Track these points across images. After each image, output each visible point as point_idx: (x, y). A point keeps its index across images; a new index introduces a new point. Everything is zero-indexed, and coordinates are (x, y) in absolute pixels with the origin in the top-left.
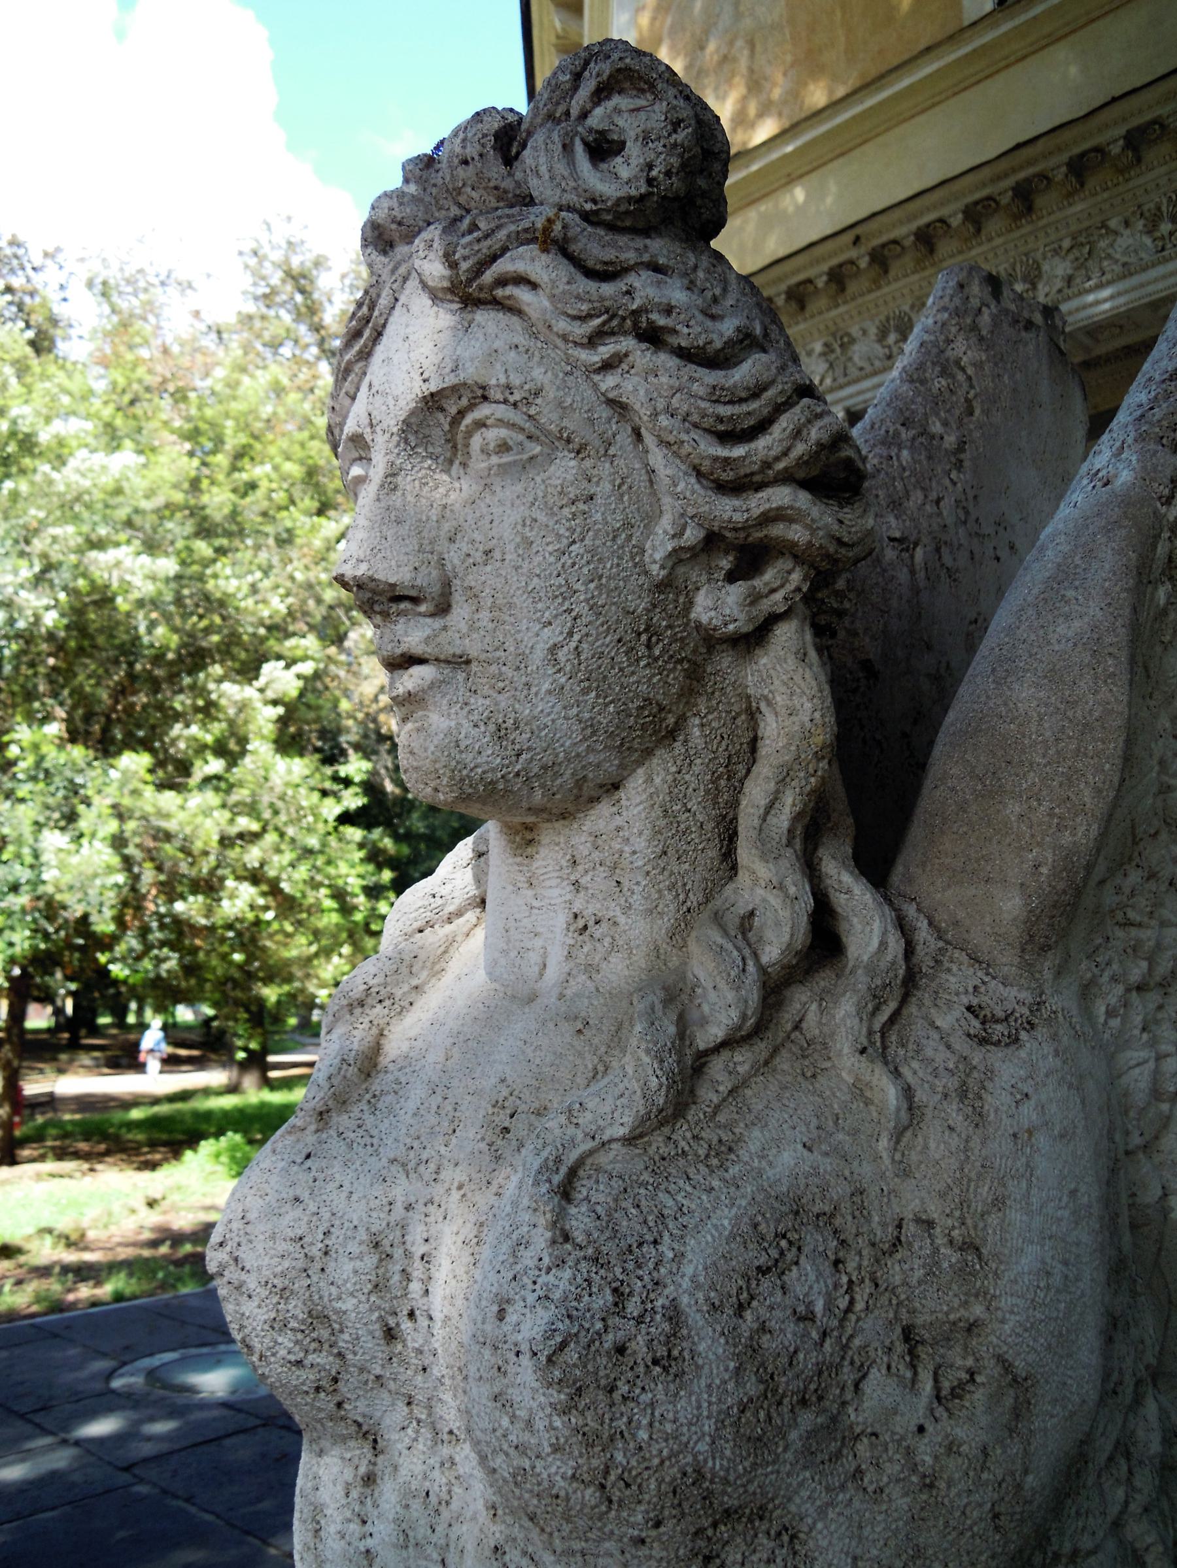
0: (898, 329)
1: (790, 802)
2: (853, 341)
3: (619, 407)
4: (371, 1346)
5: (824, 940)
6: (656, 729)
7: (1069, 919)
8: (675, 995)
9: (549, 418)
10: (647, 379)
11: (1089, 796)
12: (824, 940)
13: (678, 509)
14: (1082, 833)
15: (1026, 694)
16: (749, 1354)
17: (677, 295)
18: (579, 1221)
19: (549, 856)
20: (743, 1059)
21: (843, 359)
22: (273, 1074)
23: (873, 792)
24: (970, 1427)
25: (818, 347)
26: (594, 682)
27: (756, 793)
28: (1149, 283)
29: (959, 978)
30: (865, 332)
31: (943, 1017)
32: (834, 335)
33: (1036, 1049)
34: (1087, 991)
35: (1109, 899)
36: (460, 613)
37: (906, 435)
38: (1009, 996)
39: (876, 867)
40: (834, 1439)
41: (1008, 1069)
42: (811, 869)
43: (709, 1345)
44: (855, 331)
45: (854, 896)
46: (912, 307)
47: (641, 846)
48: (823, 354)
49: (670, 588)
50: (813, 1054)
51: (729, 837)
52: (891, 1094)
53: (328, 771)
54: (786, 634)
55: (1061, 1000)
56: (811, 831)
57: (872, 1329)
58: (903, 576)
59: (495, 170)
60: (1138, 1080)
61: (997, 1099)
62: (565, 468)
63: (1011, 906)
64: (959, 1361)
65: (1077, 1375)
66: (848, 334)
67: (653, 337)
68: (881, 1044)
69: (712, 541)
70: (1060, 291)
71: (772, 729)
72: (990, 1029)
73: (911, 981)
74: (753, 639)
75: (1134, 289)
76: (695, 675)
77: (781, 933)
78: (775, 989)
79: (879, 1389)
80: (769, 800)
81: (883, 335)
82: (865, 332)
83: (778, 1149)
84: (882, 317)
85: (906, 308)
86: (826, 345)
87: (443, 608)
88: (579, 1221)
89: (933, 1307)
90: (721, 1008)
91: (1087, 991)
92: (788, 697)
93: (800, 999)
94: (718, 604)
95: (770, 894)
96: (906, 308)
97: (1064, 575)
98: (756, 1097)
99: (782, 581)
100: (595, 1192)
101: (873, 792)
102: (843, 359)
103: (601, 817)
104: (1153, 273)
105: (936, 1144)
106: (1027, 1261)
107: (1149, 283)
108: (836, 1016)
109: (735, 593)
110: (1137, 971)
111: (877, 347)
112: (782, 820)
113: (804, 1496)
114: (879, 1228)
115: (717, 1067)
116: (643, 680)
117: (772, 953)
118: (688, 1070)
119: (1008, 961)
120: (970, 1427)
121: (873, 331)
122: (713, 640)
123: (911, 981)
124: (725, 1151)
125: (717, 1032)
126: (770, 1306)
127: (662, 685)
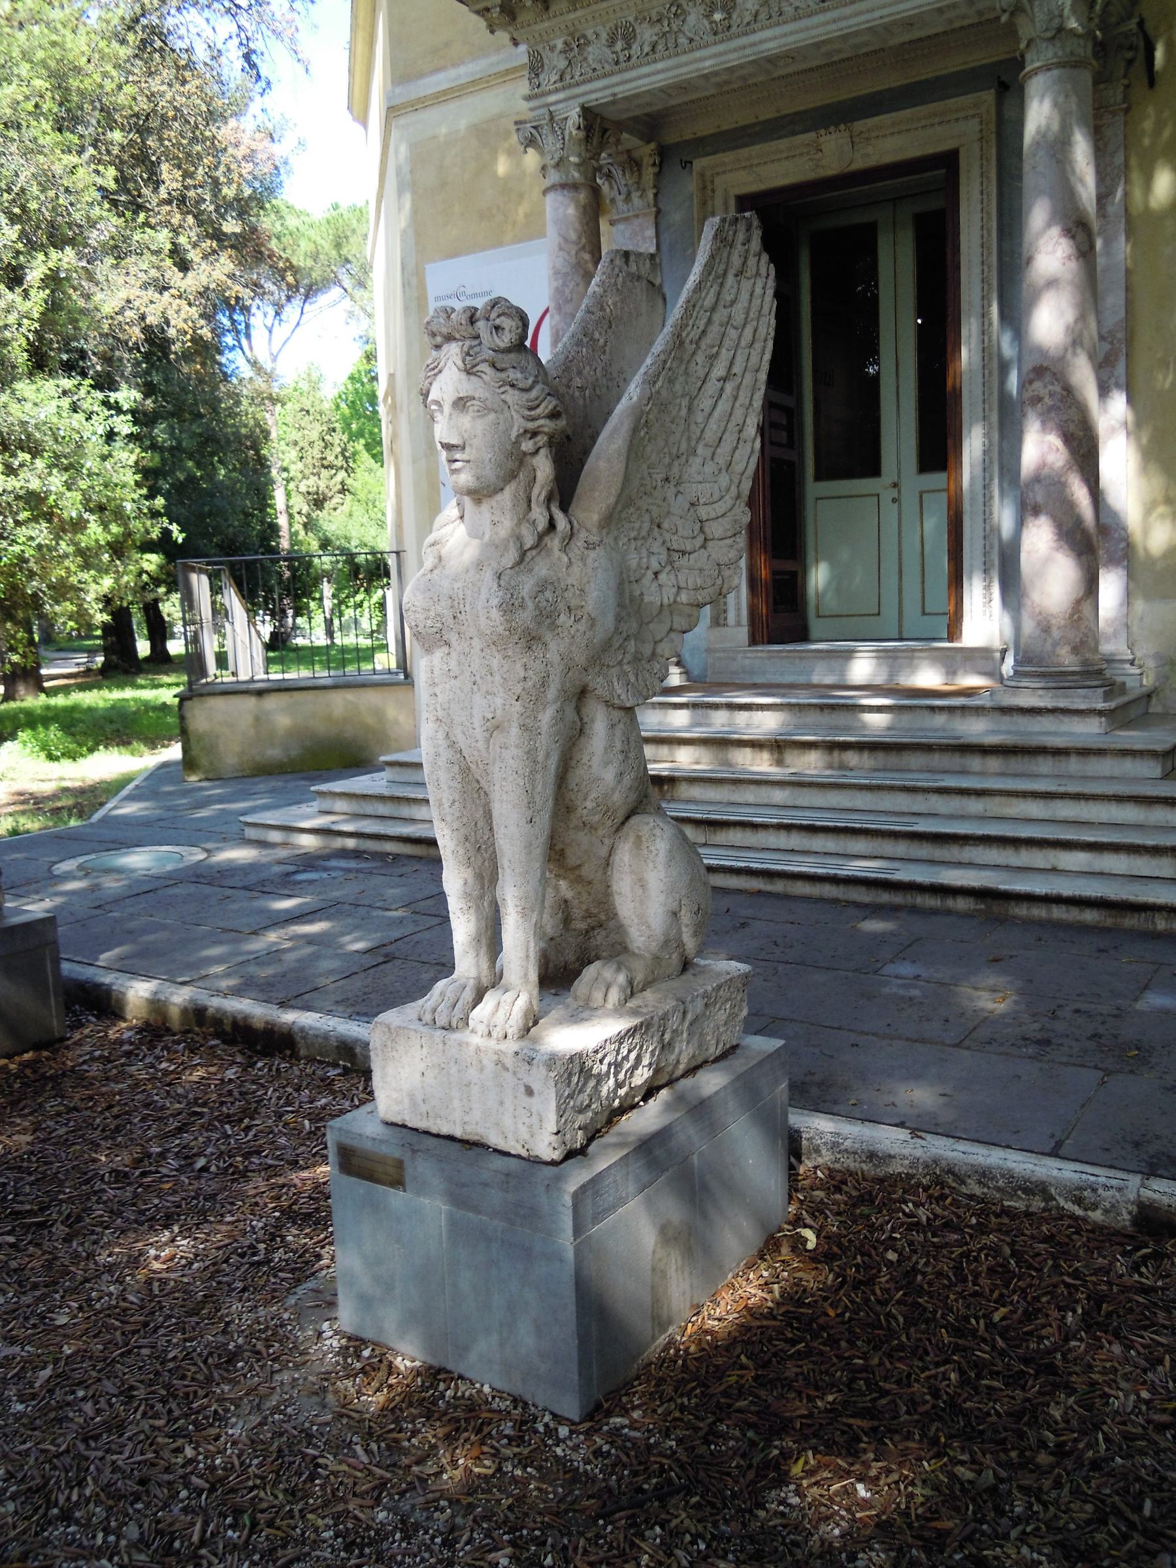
0: (624, 37)
1: (544, 494)
2: (588, 43)
3: (505, 402)
4: (451, 621)
5: (552, 526)
6: (512, 476)
7: (609, 521)
8: (519, 538)
9: (488, 403)
10: (512, 396)
11: (614, 491)
12: (552, 526)
13: (519, 425)
14: (612, 500)
15: (602, 464)
16: (537, 607)
17: (519, 375)
18: (502, 583)
19: (485, 506)
20: (534, 552)
21: (580, 58)
22: (46, 684)
23: (564, 491)
24: (582, 626)
25: (560, 44)
26: (500, 466)
27: (535, 491)
28: (813, 28)
29: (583, 535)
30: (597, 35)
31: (579, 543)
32: (572, 34)
33: (600, 551)
34: (616, 539)
35: (624, 515)
36: (468, 449)
37: (585, 340)
38: (594, 539)
39: (564, 508)
40: (553, 626)
41: (592, 554)
42: (549, 509)
43: (530, 604)
44: (590, 33)
45: (559, 516)
46: (636, 19)
47: (509, 504)
48: (565, 52)
49: (517, 443)
50: (549, 552)
51: (530, 501)
52: (566, 559)
53: (99, 395)
54: (543, 452)
55: (609, 540)
56: (549, 499)
57: (561, 606)
58: (581, 402)
59: (470, 329)
60: (634, 563)
61: (589, 561)
62: (492, 416)
63: (596, 517)
64: (580, 614)
65: (609, 622)
66: (584, 36)
67: (513, 386)
68: (565, 549)
69: (526, 431)
70: (748, 24)
71: (539, 474)
72: (589, 546)
73: (572, 535)
74: (537, 451)
75: (802, 31)
76: (521, 462)
77: (542, 524)
78: (541, 537)
79: (563, 618)
80: (539, 492)
81: (612, 42)
82: (597, 35)
83: (542, 569)
84: (612, 24)
85: (631, 19)
86: (566, 43)
87: (464, 448)
88: (502, 583)
89: (574, 603)
90: (529, 541)
91: (616, 539)
92: (543, 467)
93: (547, 539)
94: (527, 446)
95: (539, 515)
96: (631, 19)
97: (615, 430)
98: (538, 559)
99: (541, 440)
100: (505, 578)
101: (564, 491)
102: (580, 58)
103: (499, 497)
104: (816, 20)
105: (576, 570)
106: (595, 594)
107: (813, 28)
108: (554, 543)
109: (531, 443)
110: (633, 535)
111: (607, 50)
112: (542, 498)
113: (548, 637)
114: (563, 586)
115: (529, 554)
116: (510, 465)
117: (540, 529)
118: (523, 554)
119: (595, 530)
120: (582, 626)
121: (604, 36)
122: (525, 454)
123: (572, 535)
124: (531, 570)
125: (528, 546)
126: (541, 597)
127: (514, 464)
